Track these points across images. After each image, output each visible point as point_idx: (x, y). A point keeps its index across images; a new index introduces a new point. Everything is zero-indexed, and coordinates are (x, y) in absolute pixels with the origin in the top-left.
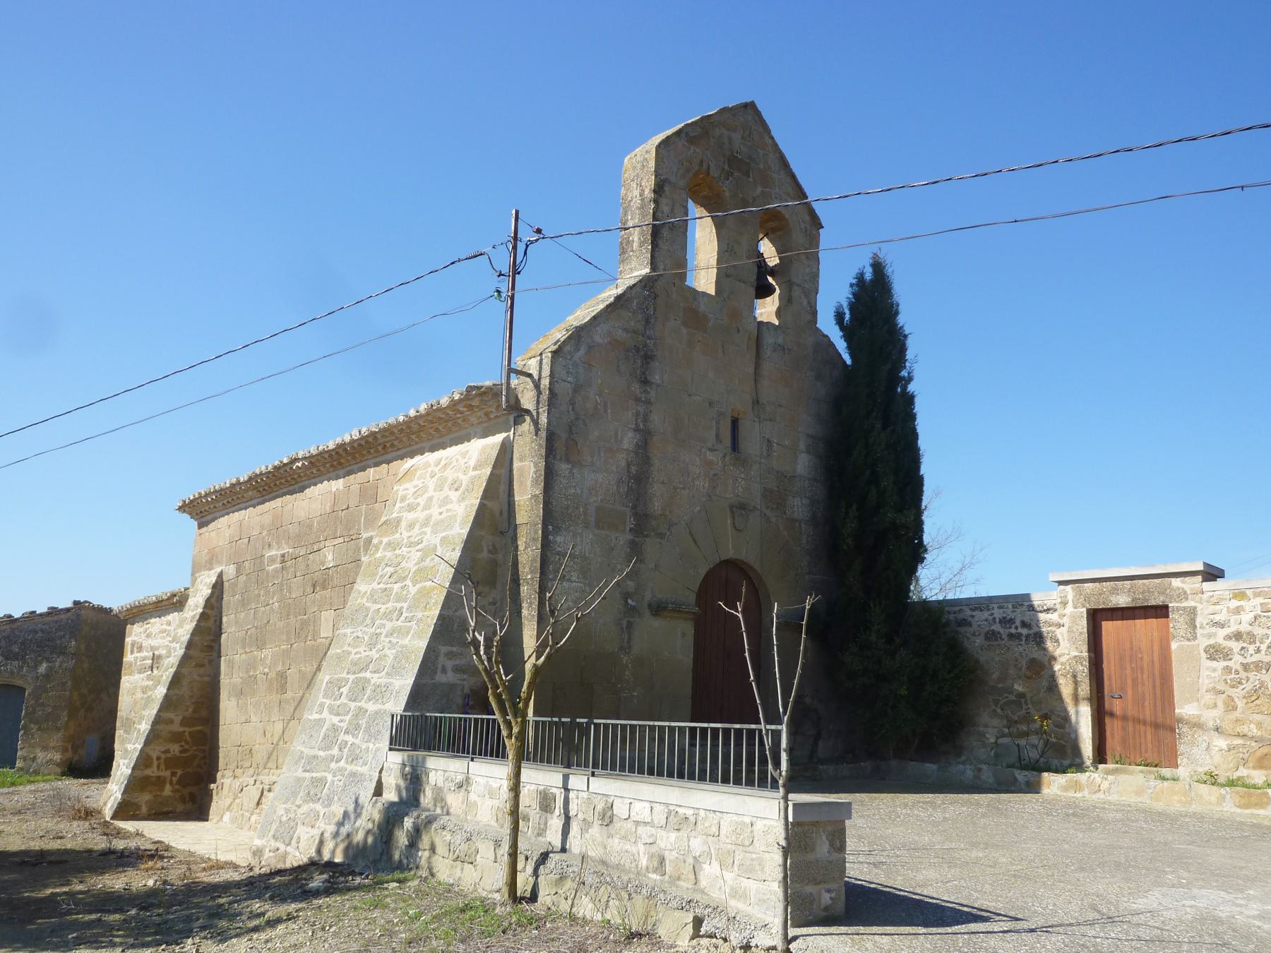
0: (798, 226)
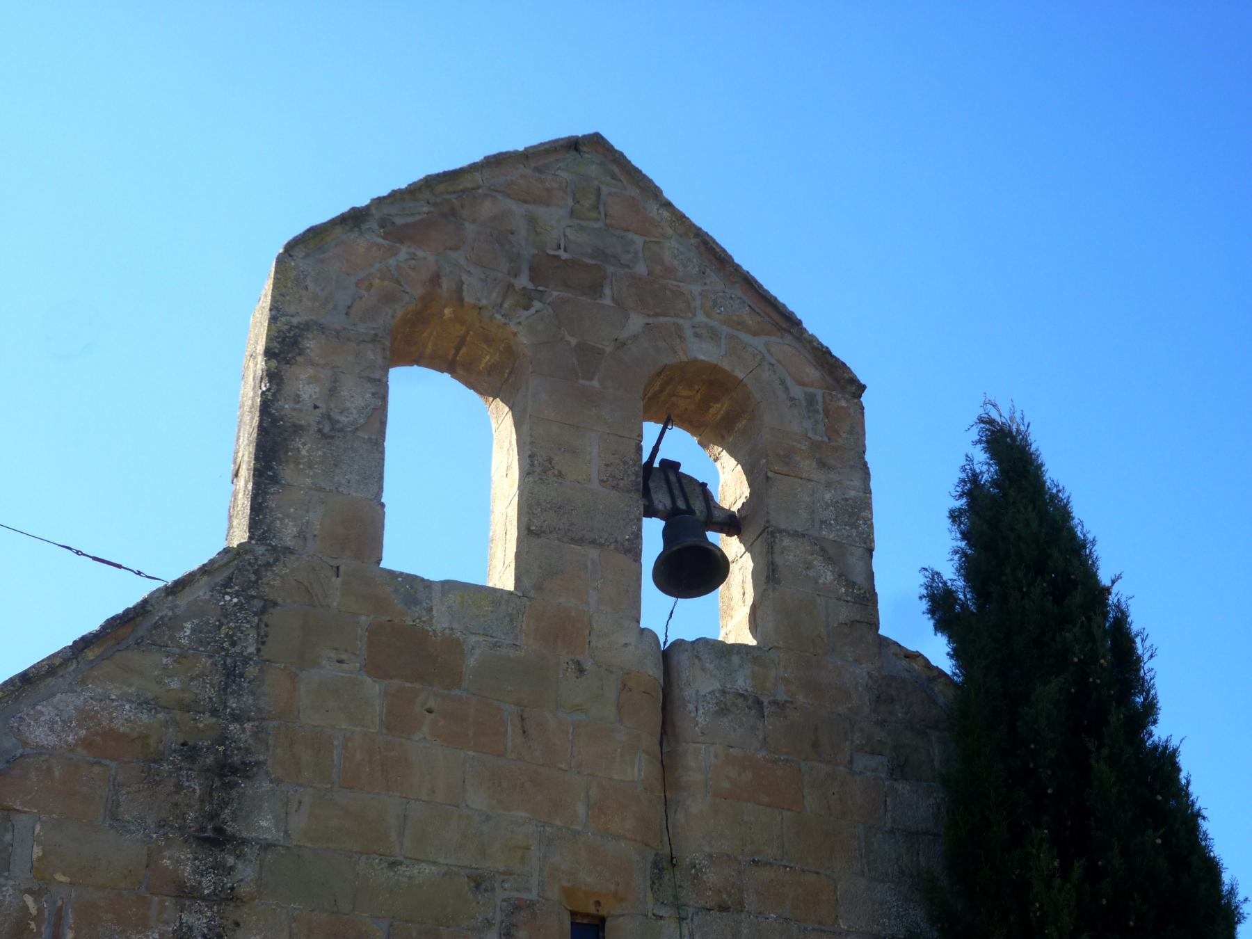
0: (803, 406)
